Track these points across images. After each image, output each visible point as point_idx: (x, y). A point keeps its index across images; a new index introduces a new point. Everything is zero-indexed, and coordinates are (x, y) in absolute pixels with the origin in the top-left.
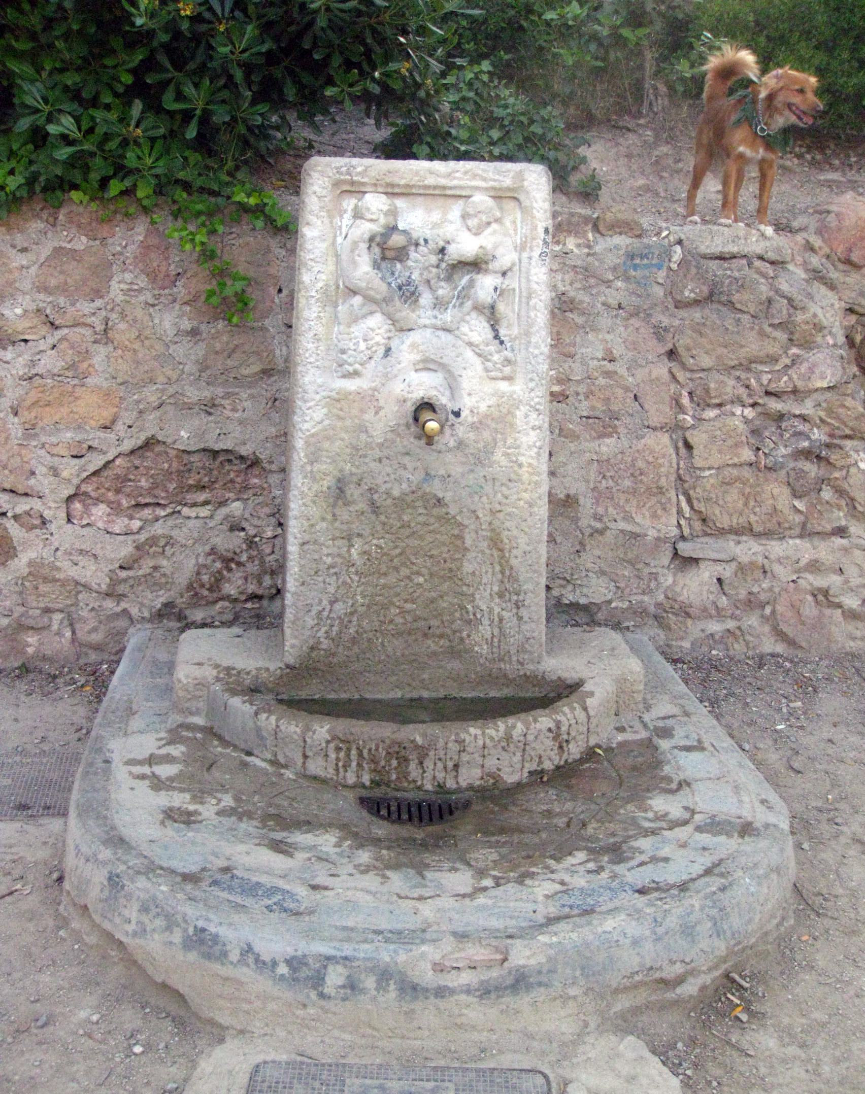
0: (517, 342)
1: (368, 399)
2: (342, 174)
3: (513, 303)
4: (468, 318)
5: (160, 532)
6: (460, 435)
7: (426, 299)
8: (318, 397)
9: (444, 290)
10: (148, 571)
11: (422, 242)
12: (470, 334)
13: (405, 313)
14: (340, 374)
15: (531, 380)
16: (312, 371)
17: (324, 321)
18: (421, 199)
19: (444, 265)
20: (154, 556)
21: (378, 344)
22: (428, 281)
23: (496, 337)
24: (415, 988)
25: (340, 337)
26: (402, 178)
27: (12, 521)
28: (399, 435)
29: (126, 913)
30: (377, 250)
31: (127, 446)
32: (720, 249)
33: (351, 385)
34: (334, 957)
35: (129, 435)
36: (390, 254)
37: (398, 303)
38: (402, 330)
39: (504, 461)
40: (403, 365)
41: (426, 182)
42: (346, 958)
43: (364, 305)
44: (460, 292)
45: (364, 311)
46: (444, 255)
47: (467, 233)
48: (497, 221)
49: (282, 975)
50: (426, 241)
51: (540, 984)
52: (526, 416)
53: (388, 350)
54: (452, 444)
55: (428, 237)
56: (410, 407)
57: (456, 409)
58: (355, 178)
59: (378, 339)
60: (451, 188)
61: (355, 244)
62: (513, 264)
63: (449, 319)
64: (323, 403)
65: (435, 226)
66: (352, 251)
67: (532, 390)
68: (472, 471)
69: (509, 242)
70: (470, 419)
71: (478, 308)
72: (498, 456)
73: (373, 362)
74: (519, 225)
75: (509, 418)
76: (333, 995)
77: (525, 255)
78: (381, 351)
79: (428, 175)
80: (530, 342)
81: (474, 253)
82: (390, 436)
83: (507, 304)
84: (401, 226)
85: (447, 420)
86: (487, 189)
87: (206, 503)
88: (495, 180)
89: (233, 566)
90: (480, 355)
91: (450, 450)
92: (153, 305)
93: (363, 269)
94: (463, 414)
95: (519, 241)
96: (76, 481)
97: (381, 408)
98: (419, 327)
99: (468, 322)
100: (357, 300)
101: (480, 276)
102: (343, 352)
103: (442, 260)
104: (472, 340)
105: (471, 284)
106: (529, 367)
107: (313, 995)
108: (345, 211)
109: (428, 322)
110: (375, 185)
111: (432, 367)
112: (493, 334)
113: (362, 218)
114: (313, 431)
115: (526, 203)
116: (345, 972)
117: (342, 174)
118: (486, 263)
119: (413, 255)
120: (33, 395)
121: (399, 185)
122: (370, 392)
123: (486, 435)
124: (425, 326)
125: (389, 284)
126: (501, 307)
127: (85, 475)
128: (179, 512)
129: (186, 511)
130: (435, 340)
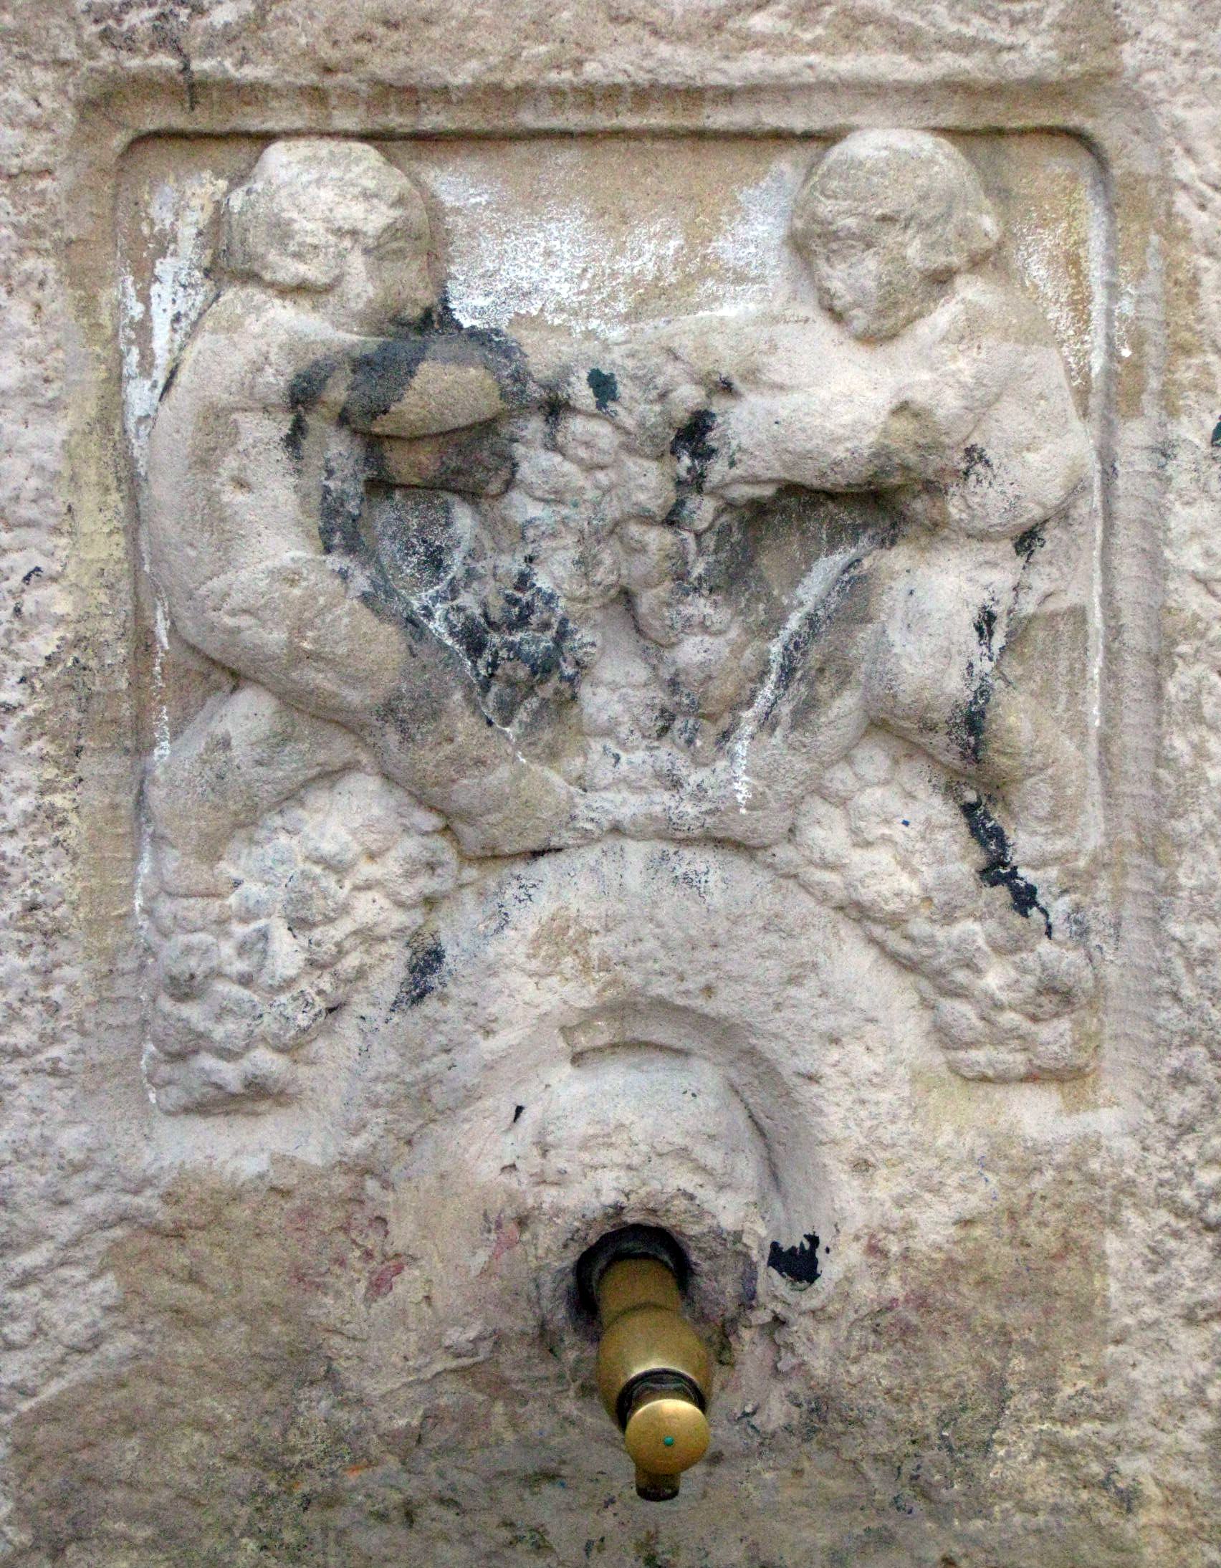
0: (1103, 887)
1: (330, 1217)
2: (129, 43)
3: (1078, 673)
4: (840, 778)
6: (819, 1366)
7: (616, 687)
8: (66, 1223)
9: (708, 641)
11: (582, 393)
12: (856, 857)
13: (513, 773)
14: (175, 1096)
15: (1181, 1078)
16: (29, 1090)
17: (75, 831)
18: (567, 156)
19: (703, 510)
21: (367, 936)
22: (626, 597)
23: (996, 870)
25: (166, 908)
26: (461, 51)
28: (499, 1387)
30: (337, 448)
33: (240, 1151)
36: (402, 463)
37: (465, 725)
38: (491, 856)
39: (1043, 1483)
40: (505, 1039)
41: (592, 70)
43: (282, 739)
44: (796, 646)
45: (288, 768)
46: (704, 454)
47: (823, 328)
48: (987, 261)
50: (603, 385)
52: (1158, 1258)
53: (426, 964)
54: (776, 1413)
55: (615, 361)
56: (550, 1253)
57: (793, 1240)
58: (201, 66)
59: (368, 909)
60: (728, 95)
61: (217, 422)
62: (1077, 489)
63: (742, 791)
64: (101, 1241)
65: (651, 298)
66: (204, 461)
67: (1186, 1128)
68: (885, 1540)
69: (1049, 369)
70: (866, 1289)
71: (890, 725)
72: (1015, 1460)
73: (347, 1025)
74: (1096, 272)
75: (1068, 1275)
77: (1135, 435)
78: (391, 969)
79: (602, 31)
80: (1170, 889)
82: (450, 1395)
83: (1045, 694)
84: (470, 307)
85: (748, 1300)
86: (919, 93)
88: (966, 46)
90: (907, 965)
91: (767, 1443)
93: (268, 550)
94: (830, 1269)
95: (1097, 362)
97: (399, 1262)
98: (588, 838)
99: (843, 802)
100: (246, 716)
101: (898, 558)
102: (185, 988)
103: (696, 482)
104: (866, 894)
105: (856, 596)
106: (1170, 1014)
108: (164, 243)
109: (627, 806)
110: (317, 96)
111: (662, 1033)
112: (978, 857)
113: (250, 277)
114: (53, 1388)
115: (1133, 159)
117: (129, 43)
118: (933, 488)
119: (535, 462)
121: (444, 93)
122: (341, 1183)
123: (955, 1361)
124: (617, 830)
125: (413, 624)
126: (1017, 718)
130: (672, 902)
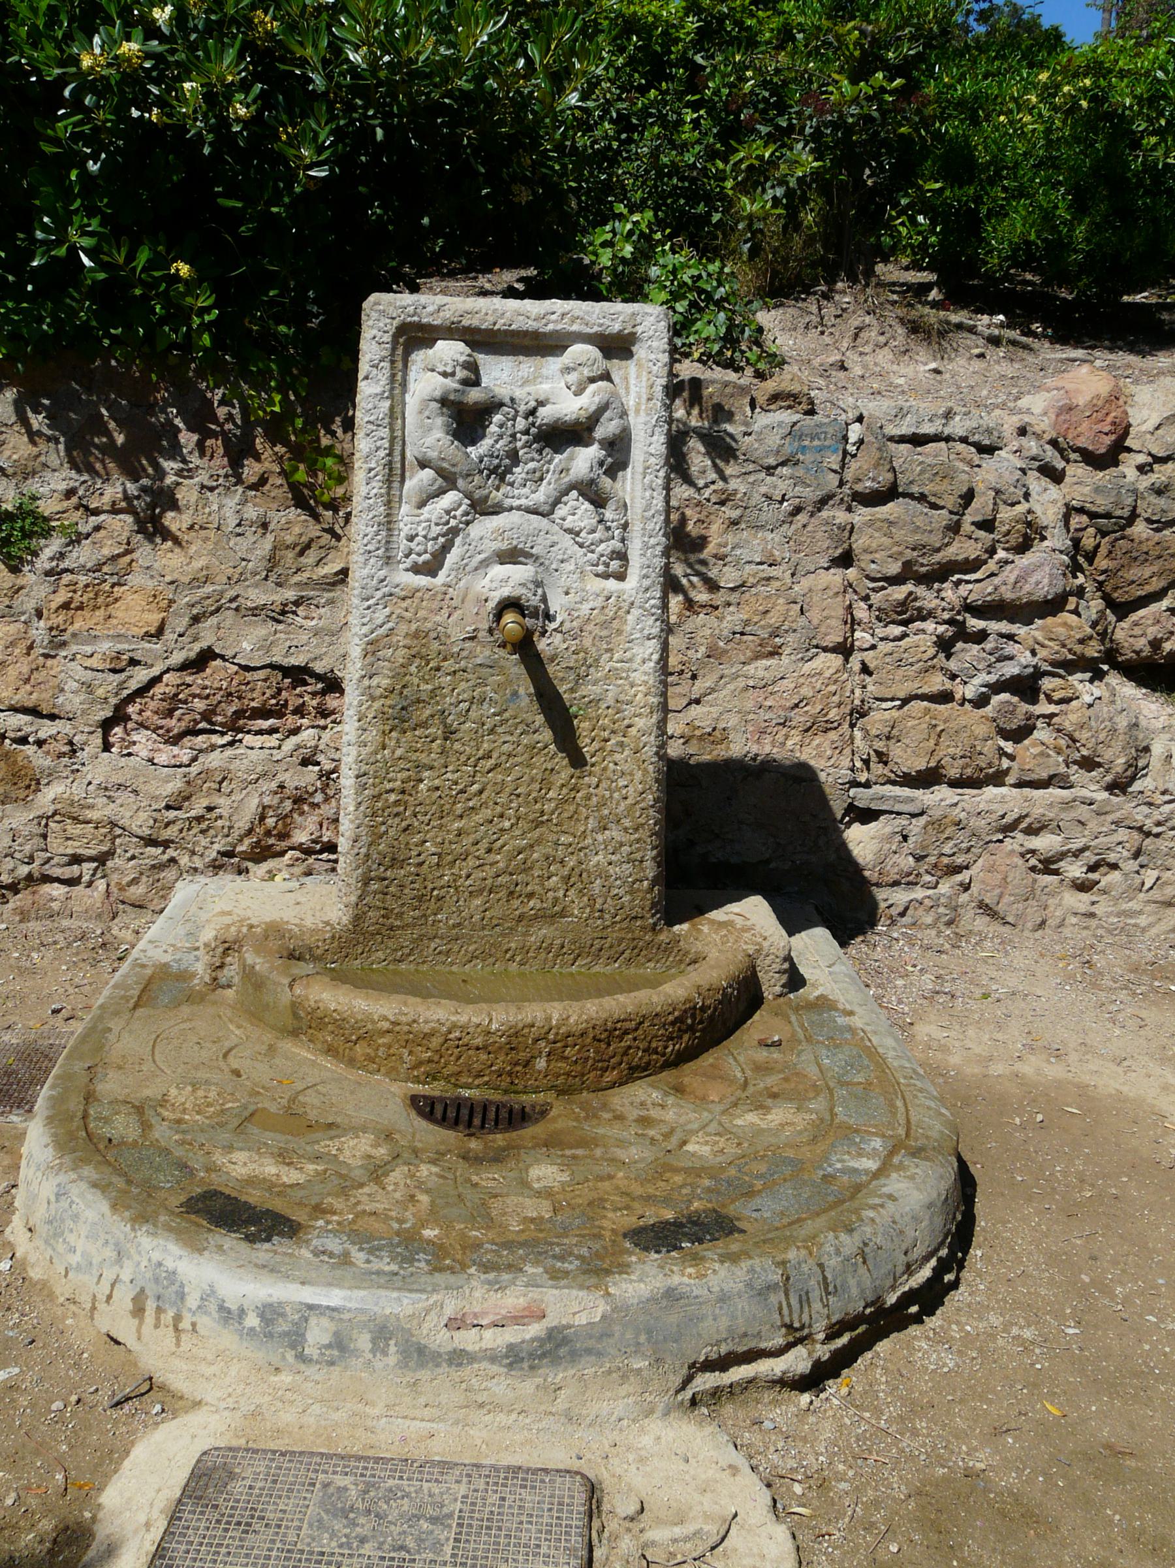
1: (440, 597)
5: (215, 764)
10: (201, 812)
20: (208, 795)
24: (421, 1350)
27: (35, 747)
29: (72, 1238)
31: (177, 658)
32: (913, 430)
34: (319, 1306)
35: (179, 645)
42: (334, 1309)
49: (252, 1329)
51: (589, 1351)
76: (315, 1357)
81: (574, 416)
87: (272, 731)
89: (306, 808)
92: (211, 489)
96: (114, 701)
107: (290, 1356)
116: (332, 1327)
120: (62, 597)
127: (125, 693)
128: (240, 741)
129: (248, 739)
